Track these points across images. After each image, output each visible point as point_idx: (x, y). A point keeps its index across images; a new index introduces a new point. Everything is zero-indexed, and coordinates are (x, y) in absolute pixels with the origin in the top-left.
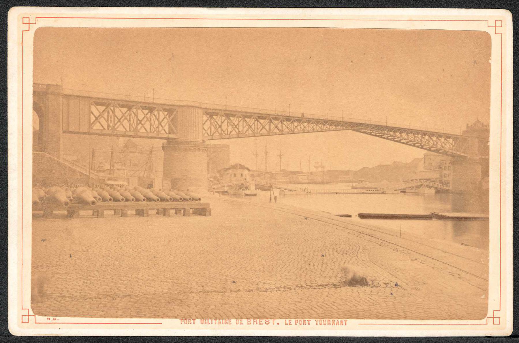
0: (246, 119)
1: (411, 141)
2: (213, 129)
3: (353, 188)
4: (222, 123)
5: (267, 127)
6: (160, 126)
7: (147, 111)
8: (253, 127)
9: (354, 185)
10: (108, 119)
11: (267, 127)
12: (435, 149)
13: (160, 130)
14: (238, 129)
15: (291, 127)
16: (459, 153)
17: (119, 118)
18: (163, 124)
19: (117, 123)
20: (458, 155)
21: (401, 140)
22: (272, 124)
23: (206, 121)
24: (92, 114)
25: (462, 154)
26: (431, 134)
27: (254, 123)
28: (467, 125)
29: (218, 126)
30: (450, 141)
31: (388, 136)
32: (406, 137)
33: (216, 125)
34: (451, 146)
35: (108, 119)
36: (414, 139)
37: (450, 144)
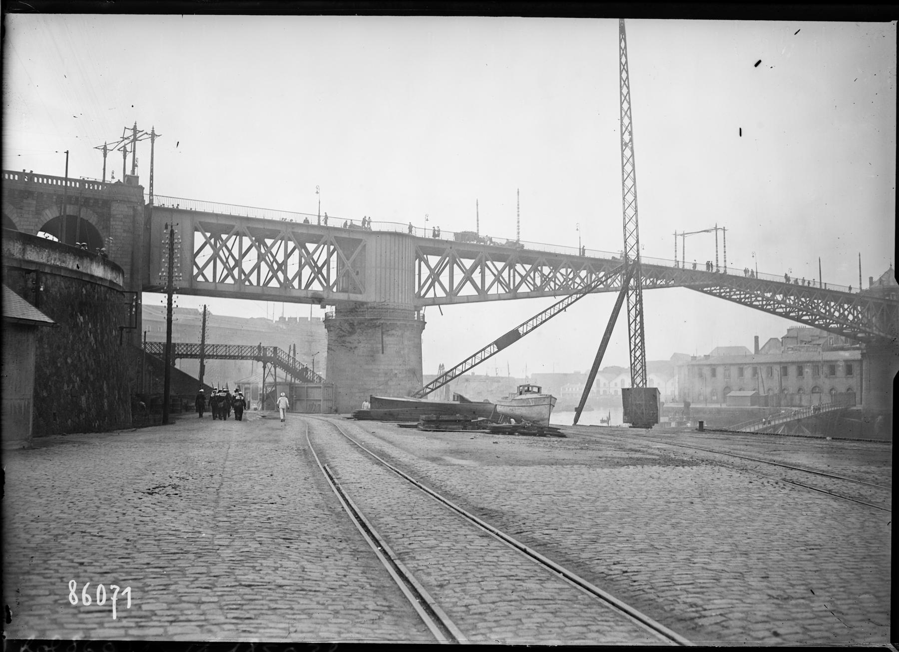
2: (220, 266)
4: (287, 256)
7: (503, 264)
19: (323, 266)
28: (871, 278)
29: (275, 266)
33: (272, 263)
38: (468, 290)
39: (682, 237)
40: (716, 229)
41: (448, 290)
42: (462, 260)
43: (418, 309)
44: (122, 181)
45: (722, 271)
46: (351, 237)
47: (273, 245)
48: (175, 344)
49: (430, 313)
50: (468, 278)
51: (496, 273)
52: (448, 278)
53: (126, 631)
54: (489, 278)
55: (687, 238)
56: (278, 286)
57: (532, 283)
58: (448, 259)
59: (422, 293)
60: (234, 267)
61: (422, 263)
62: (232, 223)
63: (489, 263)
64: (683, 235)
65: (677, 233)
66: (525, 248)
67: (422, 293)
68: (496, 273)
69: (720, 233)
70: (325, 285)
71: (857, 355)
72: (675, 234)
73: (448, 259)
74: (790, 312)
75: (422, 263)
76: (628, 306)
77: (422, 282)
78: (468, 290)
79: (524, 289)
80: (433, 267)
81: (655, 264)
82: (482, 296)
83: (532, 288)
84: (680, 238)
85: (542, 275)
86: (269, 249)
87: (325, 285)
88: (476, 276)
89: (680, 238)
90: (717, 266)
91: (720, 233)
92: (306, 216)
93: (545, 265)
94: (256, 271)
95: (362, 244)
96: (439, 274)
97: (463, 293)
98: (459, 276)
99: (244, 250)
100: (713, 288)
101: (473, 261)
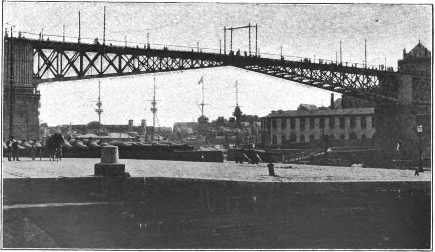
14: (180, 64)
39: (230, 31)
40: (249, 27)
41: (118, 68)
43: (35, 86)
45: (248, 54)
48: (337, 125)
49: (42, 88)
50: (92, 64)
51: (51, 67)
53: (289, 161)
54: (123, 64)
55: (235, 32)
56: (87, 53)
57: (133, 66)
64: (232, 29)
65: (227, 28)
68: (51, 67)
69: (253, 30)
70: (56, 73)
77: (56, 68)
82: (136, 71)
89: (229, 32)
90: (250, 52)
91: (253, 30)
97: (125, 71)
98: (86, 63)
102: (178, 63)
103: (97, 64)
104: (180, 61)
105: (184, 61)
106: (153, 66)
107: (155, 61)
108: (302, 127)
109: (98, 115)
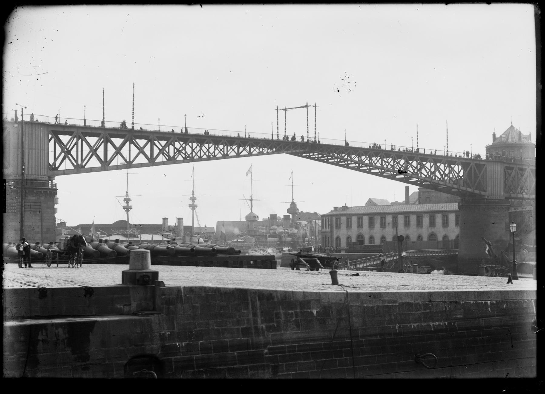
0: (88, 138)
1: (388, 171)
3: (329, 237)
5: (147, 150)
6: (193, 152)
8: (74, 152)
9: (330, 238)
10: (74, 146)
11: (147, 150)
12: (428, 183)
13: (193, 156)
14: (224, 152)
15: (168, 153)
16: (469, 190)
17: (205, 152)
18: (195, 150)
20: (470, 192)
21: (370, 170)
22: (109, 145)
23: (195, 149)
24: (154, 146)
25: (477, 192)
26: (408, 157)
27: (76, 144)
28: (494, 135)
30: (413, 164)
31: (349, 162)
32: (367, 162)
34: (416, 171)
35: (74, 146)
36: (382, 164)
37: (414, 168)
38: (94, 163)
42: (137, 140)
43: (51, 178)
44: (483, 157)
46: (142, 135)
47: (454, 167)
49: (59, 180)
52: (76, 153)
58: (102, 139)
59: (83, 164)
60: (415, 169)
61: (84, 142)
62: (149, 135)
63: (156, 142)
64: (285, 110)
66: (210, 133)
67: (83, 164)
70: (75, 164)
71: (455, 206)
72: (277, 109)
73: (102, 139)
74: (384, 172)
75: (84, 142)
76: (437, 177)
78: (94, 163)
79: (161, 158)
80: (92, 145)
81: (327, 143)
83: (167, 158)
84: (282, 113)
85: (175, 148)
86: (438, 167)
87: (75, 164)
88: (100, 152)
89: (282, 113)
92: (66, 119)
93: (176, 141)
94: (76, 159)
95: (485, 167)
96: (97, 149)
98: (111, 151)
99: (76, 146)
100: (311, 154)
101: (123, 139)
102: (221, 150)
103: (125, 151)
104: (224, 148)
105: (229, 148)
106: (192, 153)
107: (193, 148)
108: (371, 225)
109: (126, 213)
